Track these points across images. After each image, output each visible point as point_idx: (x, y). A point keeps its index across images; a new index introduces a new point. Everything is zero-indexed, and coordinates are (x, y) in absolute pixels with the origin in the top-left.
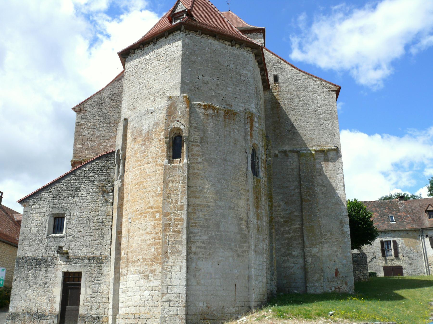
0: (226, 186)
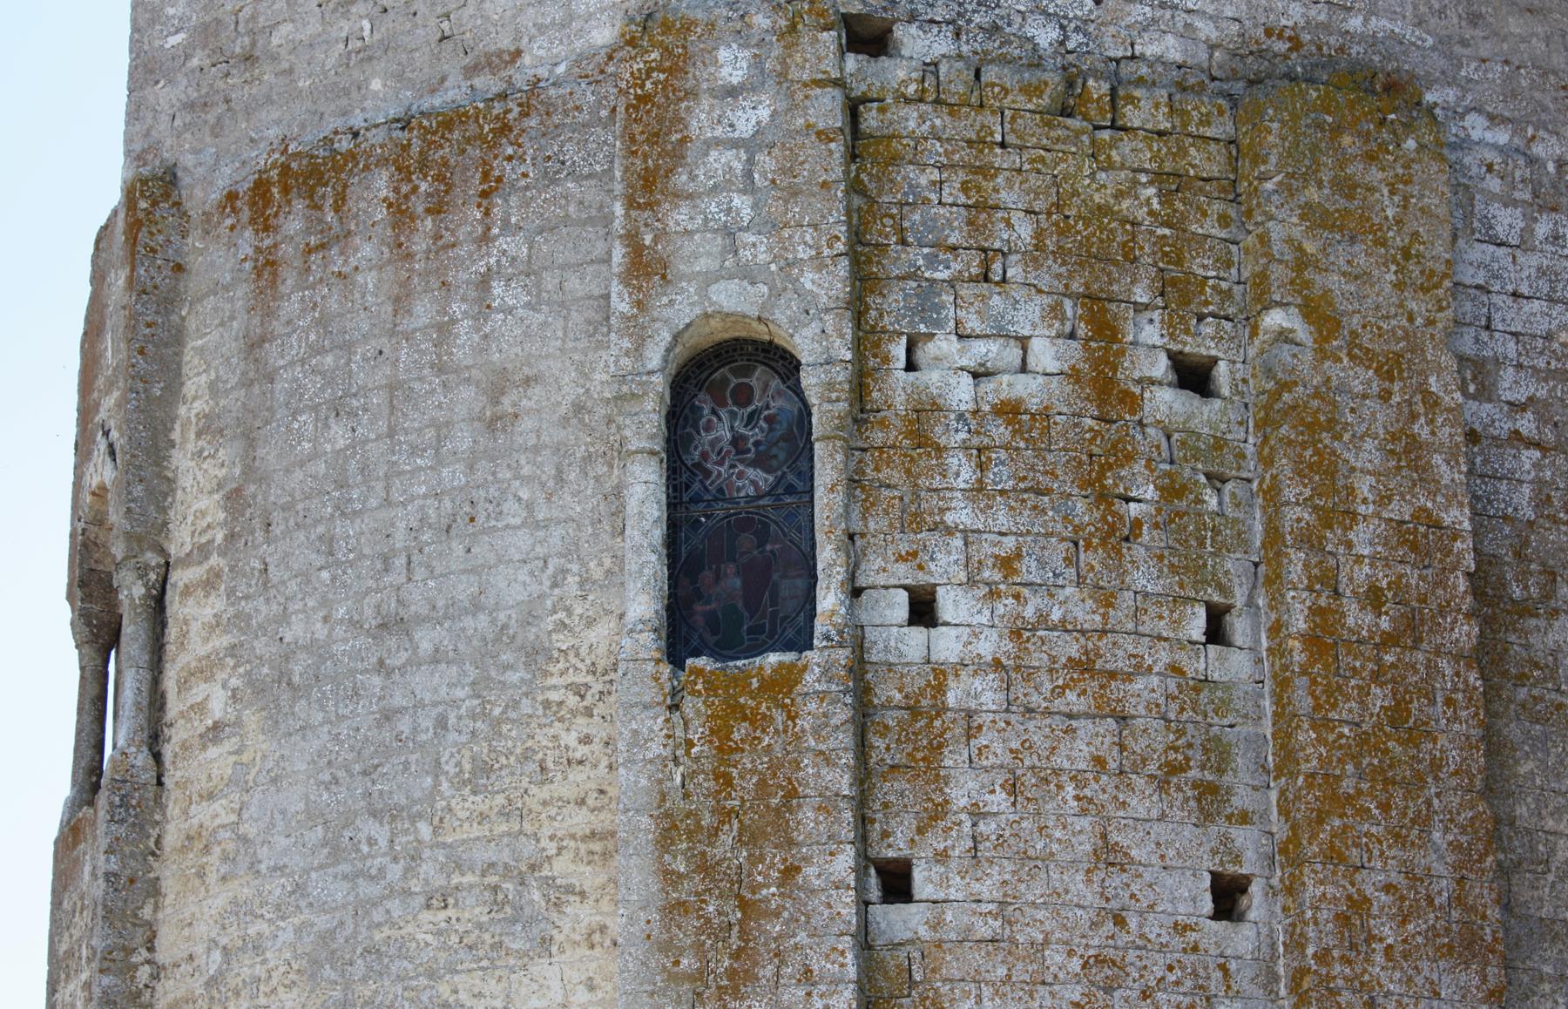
0: (395, 872)
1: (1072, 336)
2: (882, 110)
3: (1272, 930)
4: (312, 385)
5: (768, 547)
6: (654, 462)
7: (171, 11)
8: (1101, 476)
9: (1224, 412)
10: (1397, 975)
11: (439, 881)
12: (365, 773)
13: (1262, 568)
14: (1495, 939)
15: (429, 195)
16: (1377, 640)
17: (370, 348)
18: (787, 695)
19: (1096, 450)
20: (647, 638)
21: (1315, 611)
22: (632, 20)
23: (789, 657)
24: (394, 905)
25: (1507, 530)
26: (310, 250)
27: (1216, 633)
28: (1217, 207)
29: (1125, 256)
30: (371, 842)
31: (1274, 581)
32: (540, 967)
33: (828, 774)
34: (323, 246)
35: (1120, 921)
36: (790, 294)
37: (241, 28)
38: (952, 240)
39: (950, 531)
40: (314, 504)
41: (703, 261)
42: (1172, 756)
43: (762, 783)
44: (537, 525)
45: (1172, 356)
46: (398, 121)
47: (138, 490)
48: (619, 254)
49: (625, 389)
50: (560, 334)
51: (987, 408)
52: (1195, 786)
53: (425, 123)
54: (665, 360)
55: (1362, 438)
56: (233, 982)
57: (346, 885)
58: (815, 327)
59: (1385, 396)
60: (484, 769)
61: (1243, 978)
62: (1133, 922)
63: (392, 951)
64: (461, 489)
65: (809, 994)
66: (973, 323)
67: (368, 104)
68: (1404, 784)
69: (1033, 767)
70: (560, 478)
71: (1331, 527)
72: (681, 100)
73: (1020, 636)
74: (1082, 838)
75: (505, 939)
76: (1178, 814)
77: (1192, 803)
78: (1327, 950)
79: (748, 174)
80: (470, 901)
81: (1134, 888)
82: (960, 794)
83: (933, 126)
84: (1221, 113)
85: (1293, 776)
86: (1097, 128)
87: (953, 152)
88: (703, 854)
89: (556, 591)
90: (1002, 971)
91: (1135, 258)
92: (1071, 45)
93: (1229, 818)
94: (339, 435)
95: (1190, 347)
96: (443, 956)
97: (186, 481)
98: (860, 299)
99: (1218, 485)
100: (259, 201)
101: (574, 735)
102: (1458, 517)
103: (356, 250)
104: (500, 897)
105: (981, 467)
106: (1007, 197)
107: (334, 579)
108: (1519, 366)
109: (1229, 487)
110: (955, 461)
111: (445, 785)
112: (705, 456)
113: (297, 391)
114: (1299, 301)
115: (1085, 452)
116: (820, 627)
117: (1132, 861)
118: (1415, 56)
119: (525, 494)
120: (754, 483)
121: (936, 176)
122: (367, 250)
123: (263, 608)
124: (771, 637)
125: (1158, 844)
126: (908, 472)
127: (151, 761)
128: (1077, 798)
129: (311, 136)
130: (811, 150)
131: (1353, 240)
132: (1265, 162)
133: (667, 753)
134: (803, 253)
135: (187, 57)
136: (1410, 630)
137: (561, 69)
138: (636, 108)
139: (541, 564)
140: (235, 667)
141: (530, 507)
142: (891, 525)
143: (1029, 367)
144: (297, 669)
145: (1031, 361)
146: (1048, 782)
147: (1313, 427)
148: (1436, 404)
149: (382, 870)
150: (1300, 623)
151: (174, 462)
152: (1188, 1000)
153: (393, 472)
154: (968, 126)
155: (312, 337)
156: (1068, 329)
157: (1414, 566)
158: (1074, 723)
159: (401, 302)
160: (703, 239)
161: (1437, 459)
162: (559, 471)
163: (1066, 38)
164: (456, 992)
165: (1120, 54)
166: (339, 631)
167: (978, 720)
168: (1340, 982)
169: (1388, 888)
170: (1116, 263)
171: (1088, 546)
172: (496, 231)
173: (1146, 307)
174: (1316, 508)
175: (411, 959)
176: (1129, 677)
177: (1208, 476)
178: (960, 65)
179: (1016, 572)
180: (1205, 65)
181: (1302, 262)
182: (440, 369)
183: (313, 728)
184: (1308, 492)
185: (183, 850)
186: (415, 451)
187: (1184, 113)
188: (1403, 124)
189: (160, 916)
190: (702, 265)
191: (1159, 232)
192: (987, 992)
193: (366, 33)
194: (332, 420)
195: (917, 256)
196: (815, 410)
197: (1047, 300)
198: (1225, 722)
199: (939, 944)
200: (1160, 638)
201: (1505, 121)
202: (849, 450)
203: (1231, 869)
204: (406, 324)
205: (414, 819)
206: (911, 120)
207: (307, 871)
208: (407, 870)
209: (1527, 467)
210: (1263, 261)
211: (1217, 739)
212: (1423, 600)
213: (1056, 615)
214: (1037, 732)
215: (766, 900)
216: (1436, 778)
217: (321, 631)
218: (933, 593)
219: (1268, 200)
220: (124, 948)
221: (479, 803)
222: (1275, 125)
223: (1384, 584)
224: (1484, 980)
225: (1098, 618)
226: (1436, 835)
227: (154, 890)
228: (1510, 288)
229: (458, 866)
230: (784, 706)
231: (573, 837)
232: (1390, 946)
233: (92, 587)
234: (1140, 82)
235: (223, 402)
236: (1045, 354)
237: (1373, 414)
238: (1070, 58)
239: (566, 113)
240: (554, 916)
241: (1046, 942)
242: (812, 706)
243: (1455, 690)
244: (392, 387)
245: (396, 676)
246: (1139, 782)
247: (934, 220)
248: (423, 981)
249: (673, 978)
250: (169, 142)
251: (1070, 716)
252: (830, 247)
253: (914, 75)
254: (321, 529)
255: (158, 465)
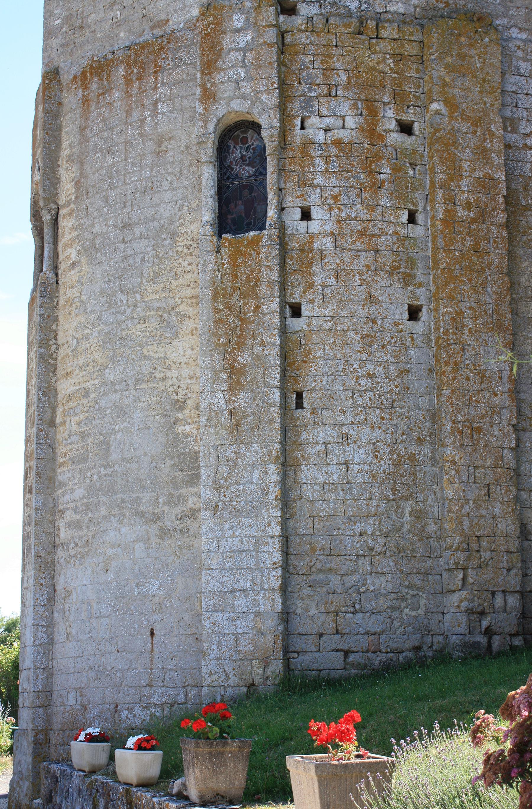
0: (129, 311)
1: (361, 115)
2: (292, 35)
3: (430, 324)
4: (101, 143)
5: (253, 194)
6: (212, 166)
7: (56, 12)
8: (371, 165)
9: (416, 140)
10: (473, 338)
11: (143, 314)
12: (119, 278)
13: (429, 196)
14: (509, 325)
15: (137, 73)
16: (469, 221)
17: (119, 129)
18: (256, 246)
19: (369, 156)
20: (209, 228)
21: (446, 211)
22: (203, 6)
23: (258, 233)
24: (129, 323)
25: (521, 180)
26: (99, 95)
27: (412, 220)
28: (415, 65)
29: (381, 85)
30: (121, 301)
31: (433, 201)
32: (176, 343)
33: (270, 274)
34: (103, 94)
35: (374, 322)
36: (258, 103)
37: (79, 17)
38: (317, 82)
39: (315, 187)
40: (102, 185)
41: (228, 93)
42: (394, 264)
43: (248, 277)
44: (174, 190)
45: (397, 121)
46: (127, 47)
47: (47, 182)
48: (198, 91)
49: (201, 140)
50: (181, 121)
51: (329, 142)
52: (402, 274)
53: (136, 47)
54: (215, 129)
55: (465, 148)
56: (80, 350)
57: (114, 316)
58: (267, 115)
59: (474, 133)
60: (157, 275)
61: (419, 341)
62: (379, 322)
63: (128, 338)
64: (148, 178)
65: (264, 350)
66: (324, 112)
67: (120, 42)
68: (478, 272)
69: (344, 269)
70: (181, 173)
71: (453, 181)
72: (220, 34)
73: (340, 223)
74: (362, 293)
75: (164, 333)
76: (396, 284)
77: (401, 280)
78: (448, 330)
79: (243, 61)
80: (153, 320)
81: (380, 310)
82: (318, 279)
83: (311, 40)
84: (417, 31)
85: (437, 270)
86: (371, 38)
87: (318, 50)
88: (228, 302)
89: (180, 212)
90: (332, 340)
91: (385, 86)
92: (363, 8)
93: (415, 285)
94: (109, 160)
95: (404, 117)
96: (144, 339)
97: (63, 179)
98: (284, 104)
99: (414, 167)
100: (83, 79)
101: (186, 262)
102: (501, 176)
103: (114, 94)
104: (163, 319)
105: (327, 163)
106: (337, 65)
107: (108, 211)
108: (528, 120)
109: (418, 167)
110: (318, 161)
111: (144, 281)
112: (231, 163)
113: (96, 146)
114: (443, 99)
115: (364, 157)
116: (269, 221)
117: (379, 301)
118: (492, 6)
119: (169, 179)
120: (248, 172)
121: (312, 59)
122: (117, 94)
123: (87, 222)
124: (254, 226)
125: (389, 295)
126: (301, 166)
127: (54, 276)
128: (360, 279)
129: (101, 54)
130: (265, 51)
131: (464, 76)
132: (431, 49)
133: (216, 268)
134: (263, 88)
135: (62, 28)
136: (482, 216)
137: (181, 26)
138: (205, 38)
139: (175, 203)
140: (79, 242)
141: (171, 183)
142: (295, 185)
143: (346, 126)
144: (98, 242)
145: (346, 124)
146: (349, 274)
147: (447, 145)
148: (494, 135)
149: (124, 311)
150: (441, 216)
151: (60, 172)
152: (399, 349)
153: (127, 172)
154: (322, 40)
155: (100, 126)
156: (359, 112)
157: (484, 194)
158: (359, 253)
159: (128, 113)
160: (228, 85)
161: (493, 155)
162: (181, 170)
163: (361, 6)
164: (148, 352)
165: (381, 11)
166: (110, 229)
167: (325, 253)
168: (452, 341)
169: (470, 308)
170: (377, 88)
171: (365, 190)
172: (159, 85)
173: (389, 103)
174: (447, 174)
175: (134, 341)
176: (380, 236)
177: (410, 164)
178: (321, 17)
179: (339, 200)
180: (413, 14)
181: (445, 85)
182: (141, 135)
183: (102, 262)
184: (444, 169)
185: (65, 305)
186: (134, 165)
187: (403, 32)
188: (484, 33)
189: (59, 328)
190: (227, 94)
191: (393, 76)
192: (327, 347)
193: (119, 16)
194: (107, 155)
195: (305, 88)
196: (267, 145)
197: (352, 102)
198: (414, 251)
199: (310, 332)
200: (391, 222)
201: (526, 30)
202: (279, 159)
203: (415, 303)
204: (130, 120)
205: (134, 293)
206: (303, 38)
207: (101, 312)
208: (132, 311)
209: (529, 157)
210: (430, 85)
211: (411, 258)
212: (486, 206)
213: (353, 215)
214: (346, 257)
215: (249, 318)
216: (490, 269)
217: (105, 229)
218: (310, 209)
219: (432, 62)
220: (46, 339)
221: (155, 287)
222: (436, 35)
223: (472, 200)
224: (505, 339)
225: (368, 216)
226: (489, 289)
227: (56, 319)
228: (525, 92)
229: (149, 309)
230: (255, 250)
231: (186, 298)
232: (471, 328)
233: (36, 216)
234: (388, 21)
235: (74, 150)
236: (350, 122)
237: (470, 140)
238: (363, 13)
239: (182, 41)
240: (180, 325)
241: (348, 330)
242: (265, 250)
243: (497, 238)
244: (126, 142)
245: (128, 244)
246: (382, 273)
247: (311, 75)
248: (138, 348)
249: (218, 345)
250: (56, 59)
251: (358, 251)
252: (272, 86)
253: (304, 22)
254: (104, 194)
255: (54, 173)
